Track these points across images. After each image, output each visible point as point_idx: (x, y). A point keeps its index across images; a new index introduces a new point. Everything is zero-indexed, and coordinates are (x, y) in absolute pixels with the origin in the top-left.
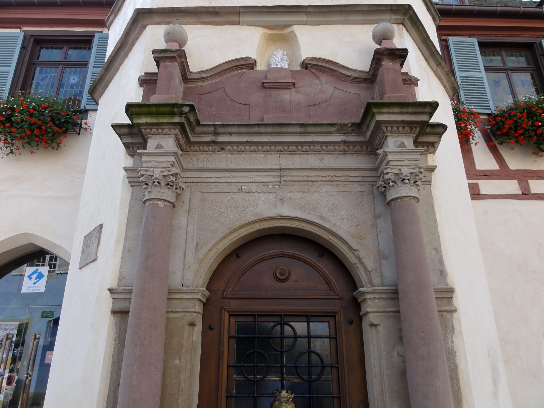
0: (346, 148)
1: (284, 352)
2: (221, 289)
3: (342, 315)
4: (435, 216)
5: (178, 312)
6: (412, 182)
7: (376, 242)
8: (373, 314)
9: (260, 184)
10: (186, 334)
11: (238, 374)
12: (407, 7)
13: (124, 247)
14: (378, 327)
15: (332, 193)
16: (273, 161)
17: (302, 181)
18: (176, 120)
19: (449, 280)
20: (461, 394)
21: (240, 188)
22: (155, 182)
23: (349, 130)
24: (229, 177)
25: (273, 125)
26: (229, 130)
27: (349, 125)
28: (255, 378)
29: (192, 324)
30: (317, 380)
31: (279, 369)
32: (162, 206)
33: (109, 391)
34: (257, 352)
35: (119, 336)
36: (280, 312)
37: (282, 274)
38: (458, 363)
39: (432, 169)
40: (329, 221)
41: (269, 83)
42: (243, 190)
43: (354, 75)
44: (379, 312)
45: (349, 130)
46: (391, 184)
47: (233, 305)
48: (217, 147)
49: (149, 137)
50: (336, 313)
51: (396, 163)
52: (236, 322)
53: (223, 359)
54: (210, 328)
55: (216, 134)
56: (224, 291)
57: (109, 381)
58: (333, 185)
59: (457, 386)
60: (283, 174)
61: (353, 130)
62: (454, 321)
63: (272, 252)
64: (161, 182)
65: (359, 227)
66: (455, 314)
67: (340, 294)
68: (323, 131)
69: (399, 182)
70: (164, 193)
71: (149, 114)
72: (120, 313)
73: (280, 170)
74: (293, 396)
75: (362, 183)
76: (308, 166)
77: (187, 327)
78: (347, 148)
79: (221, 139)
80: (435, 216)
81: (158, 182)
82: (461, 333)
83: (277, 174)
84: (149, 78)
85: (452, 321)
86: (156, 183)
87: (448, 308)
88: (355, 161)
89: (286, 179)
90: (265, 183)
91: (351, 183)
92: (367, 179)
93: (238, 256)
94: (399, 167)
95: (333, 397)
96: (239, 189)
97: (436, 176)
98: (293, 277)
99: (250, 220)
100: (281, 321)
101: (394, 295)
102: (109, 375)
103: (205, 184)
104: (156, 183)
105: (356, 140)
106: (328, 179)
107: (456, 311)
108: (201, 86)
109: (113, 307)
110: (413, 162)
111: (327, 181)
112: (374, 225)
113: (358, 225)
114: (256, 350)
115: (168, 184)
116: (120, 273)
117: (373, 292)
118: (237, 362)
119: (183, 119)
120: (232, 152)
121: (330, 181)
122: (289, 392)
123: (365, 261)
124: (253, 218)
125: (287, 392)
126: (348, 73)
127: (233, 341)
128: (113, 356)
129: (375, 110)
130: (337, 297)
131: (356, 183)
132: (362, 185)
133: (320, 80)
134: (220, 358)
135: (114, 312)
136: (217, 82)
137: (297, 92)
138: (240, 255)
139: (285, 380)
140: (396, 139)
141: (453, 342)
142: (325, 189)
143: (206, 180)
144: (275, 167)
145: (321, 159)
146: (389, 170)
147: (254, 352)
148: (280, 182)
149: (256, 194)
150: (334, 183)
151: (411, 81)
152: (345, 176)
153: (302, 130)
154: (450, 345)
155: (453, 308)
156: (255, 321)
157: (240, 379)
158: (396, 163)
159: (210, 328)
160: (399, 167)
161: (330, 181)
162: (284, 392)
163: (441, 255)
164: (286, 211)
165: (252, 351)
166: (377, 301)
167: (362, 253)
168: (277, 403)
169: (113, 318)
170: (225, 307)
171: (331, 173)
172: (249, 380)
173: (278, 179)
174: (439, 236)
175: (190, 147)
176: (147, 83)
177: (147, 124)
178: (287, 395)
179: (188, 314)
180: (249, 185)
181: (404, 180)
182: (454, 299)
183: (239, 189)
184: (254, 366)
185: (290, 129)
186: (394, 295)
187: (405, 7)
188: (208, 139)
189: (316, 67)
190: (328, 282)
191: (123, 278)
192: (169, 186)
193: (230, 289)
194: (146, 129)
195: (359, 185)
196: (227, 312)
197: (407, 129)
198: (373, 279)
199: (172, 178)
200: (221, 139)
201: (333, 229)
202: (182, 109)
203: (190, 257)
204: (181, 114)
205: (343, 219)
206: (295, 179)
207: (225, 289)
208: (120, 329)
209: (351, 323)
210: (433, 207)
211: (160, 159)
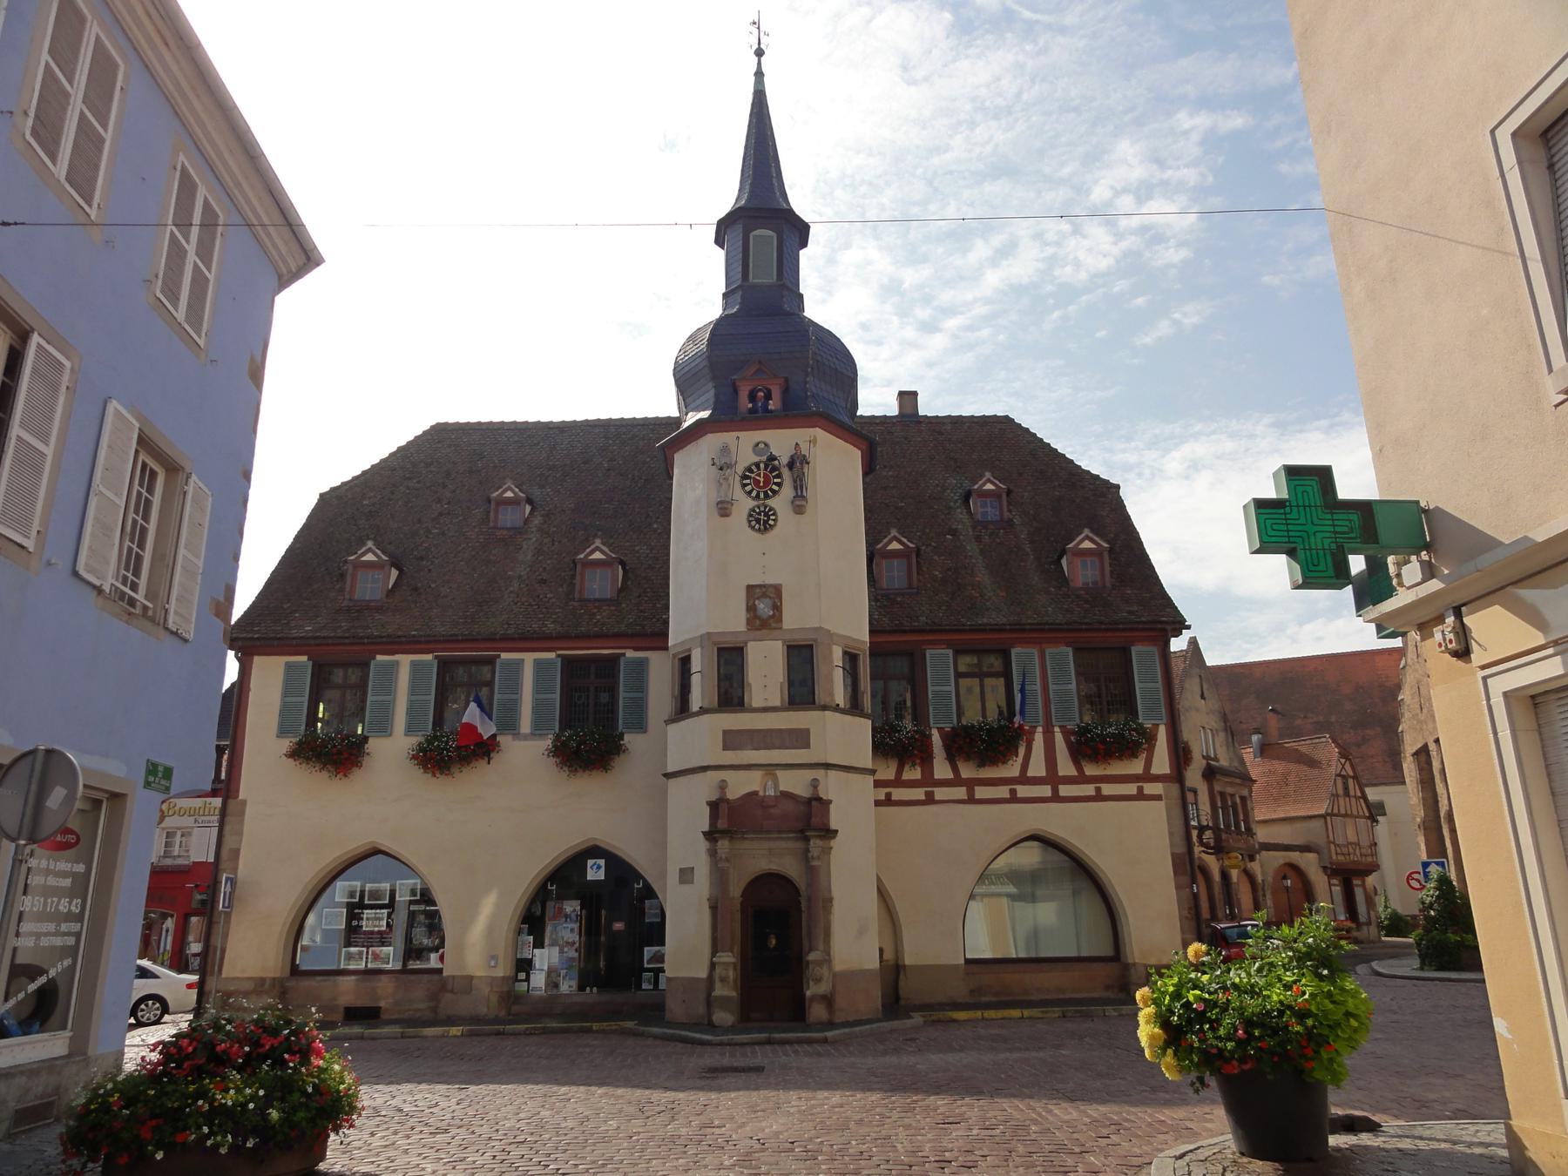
72: (714, 908)
78: (797, 839)
88: (799, 845)
97: (833, 852)
189: (786, 795)
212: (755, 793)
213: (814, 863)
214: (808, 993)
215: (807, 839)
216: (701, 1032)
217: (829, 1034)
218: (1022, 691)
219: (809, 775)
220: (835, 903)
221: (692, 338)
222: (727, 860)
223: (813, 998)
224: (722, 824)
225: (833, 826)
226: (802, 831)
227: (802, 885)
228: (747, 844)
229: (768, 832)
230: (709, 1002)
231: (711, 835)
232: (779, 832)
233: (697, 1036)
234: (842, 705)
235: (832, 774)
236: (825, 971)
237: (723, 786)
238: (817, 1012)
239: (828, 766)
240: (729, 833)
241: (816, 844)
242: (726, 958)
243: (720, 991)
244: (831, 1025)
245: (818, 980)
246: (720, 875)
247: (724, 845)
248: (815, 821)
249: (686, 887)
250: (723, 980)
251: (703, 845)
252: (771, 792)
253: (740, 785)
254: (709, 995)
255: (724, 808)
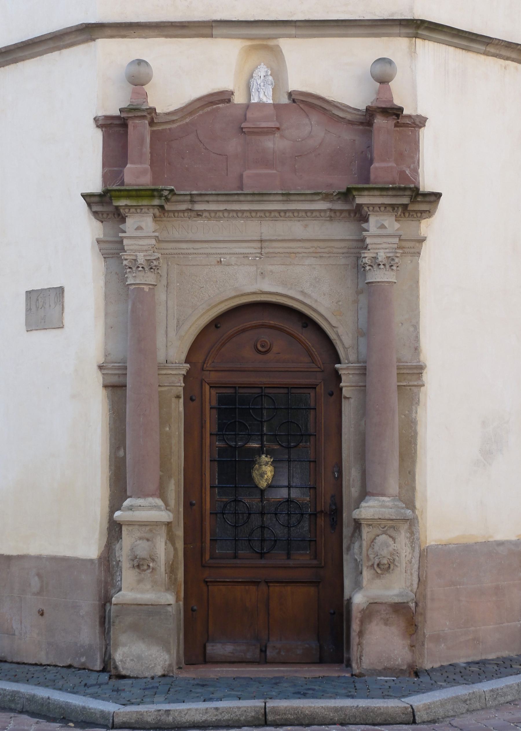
0: (333, 215)
1: (264, 421)
2: (201, 361)
3: (323, 387)
4: (418, 291)
5: (165, 386)
6: (388, 266)
7: (356, 318)
8: (346, 388)
9: (240, 256)
10: (173, 405)
11: (219, 440)
12: (419, 22)
13: (106, 323)
14: (350, 399)
15: (315, 266)
16: (254, 229)
17: (284, 253)
18: (156, 202)
19: (422, 358)
20: (416, 456)
21: (219, 260)
22: (139, 267)
23: (335, 198)
24: (207, 248)
25: (253, 194)
26: (207, 198)
27: (334, 194)
28: (236, 445)
29: (178, 397)
30: (295, 446)
31: (260, 437)
32: (147, 290)
33: (110, 452)
34: (238, 421)
35: (113, 407)
36: (261, 384)
37: (263, 346)
38: (418, 430)
39: (422, 240)
40: (310, 297)
41: (249, 128)
42: (223, 263)
43: (349, 117)
44: (354, 386)
45: (335, 198)
46: (368, 268)
47: (213, 377)
48: (193, 214)
49: (127, 216)
50: (317, 385)
51: (374, 246)
52: (217, 393)
53: (205, 428)
54: (192, 400)
55: (192, 202)
56: (204, 363)
57: (109, 445)
58: (316, 257)
59: (414, 449)
60: (265, 244)
61: (339, 198)
62: (421, 394)
63: (254, 323)
64: (145, 267)
65: (341, 303)
66: (422, 388)
67: (322, 367)
68: (307, 199)
69: (375, 267)
70: (148, 277)
71: (129, 197)
72: (116, 388)
73: (261, 241)
74: (272, 460)
75: (347, 255)
76: (290, 238)
77: (174, 400)
78: (333, 215)
79: (198, 207)
80: (418, 291)
81: (143, 267)
82: (425, 405)
83: (258, 245)
84: (109, 122)
85: (419, 395)
86: (140, 269)
87: (416, 383)
88: (341, 231)
89: (267, 250)
90: (246, 256)
91: (336, 255)
92: (352, 251)
93: (217, 327)
94: (377, 251)
95: (310, 461)
96: (218, 262)
97: (426, 249)
98: (275, 349)
99: (230, 296)
100: (262, 392)
101: (363, 372)
102: (108, 440)
103: (181, 256)
104: (140, 269)
105: (342, 208)
106: (311, 250)
107: (424, 385)
108: (170, 129)
109: (103, 381)
110: (391, 245)
111: (309, 253)
112: (356, 302)
113: (339, 301)
114: (237, 420)
115: (151, 268)
116: (106, 350)
117: (347, 368)
118: (218, 431)
119: (163, 201)
120: (209, 219)
121: (313, 253)
122: (269, 456)
123: (343, 338)
124: (233, 294)
125: (266, 457)
126: (341, 114)
127: (215, 412)
128: (109, 424)
129: (355, 193)
130: (318, 370)
131: (342, 255)
132: (347, 257)
133: (309, 120)
134: (202, 426)
135: (105, 386)
136: (187, 124)
137: (282, 137)
138: (219, 325)
139: (264, 447)
140: (378, 218)
141: (416, 413)
142: (307, 262)
143: (183, 251)
144: (256, 238)
145: (306, 226)
146: (366, 255)
147: (235, 421)
148: (261, 254)
149: (236, 267)
150: (318, 255)
151: (416, 124)
152: (330, 247)
153: (285, 198)
154: (414, 415)
155: (420, 383)
156: (236, 393)
157: (222, 446)
158: (374, 246)
159: (192, 400)
160: (377, 251)
161: (313, 253)
162: (263, 456)
163: (419, 332)
164: (267, 288)
165: (233, 421)
166: (351, 376)
167: (341, 330)
168: (257, 465)
169: (104, 391)
170: (206, 380)
171: (315, 244)
172: (231, 446)
173: (259, 251)
174: (419, 312)
175: (164, 214)
176: (106, 127)
177: (126, 206)
178: (267, 459)
179: (174, 388)
180: (228, 257)
181: (380, 265)
182: (424, 374)
183: (218, 262)
184: (235, 435)
185: (271, 198)
186: (363, 372)
187: (416, 23)
188: (184, 207)
189: (306, 103)
190: (310, 355)
191: (109, 354)
192: (152, 270)
193: (210, 362)
194: (124, 209)
195: (343, 257)
196: (208, 384)
197: (390, 209)
198: (349, 356)
199: (155, 263)
200: (198, 207)
201: (314, 306)
202: (162, 192)
203: (172, 333)
204: (160, 196)
205: (324, 295)
206: (277, 250)
207: (205, 360)
208: (112, 401)
209: (331, 394)
210: (418, 282)
211: (141, 242)
212: (222, 98)
213: (378, 276)
214: (359, 599)
215: (360, 216)
216: (83, 689)
217: (419, 701)
218: (244, 487)
219: (366, 50)
220: (432, 378)
221: (82, 24)
222: (151, 266)
223: (371, 611)
224: (137, 173)
225: (428, 183)
226: (347, 195)
227: (344, 335)
228: (200, 229)
229: (261, 196)
230: (104, 619)
231: (106, 204)
232: (287, 196)
233: (76, 701)
234: (206, 384)
235: (430, 53)
236: (401, 544)
237: (138, 77)
238: (378, 644)
239: (418, 28)
240: (158, 198)
241: (383, 228)
242: (154, 511)
243: (131, 590)
244: (416, 676)
245: (384, 568)
246: (130, 304)
247: (141, 227)
248: (382, 169)
249: (44, 338)
250: (140, 565)
251: (86, 229)
252: (264, 95)
253: (184, 76)
254: (105, 601)
255: (139, 132)
